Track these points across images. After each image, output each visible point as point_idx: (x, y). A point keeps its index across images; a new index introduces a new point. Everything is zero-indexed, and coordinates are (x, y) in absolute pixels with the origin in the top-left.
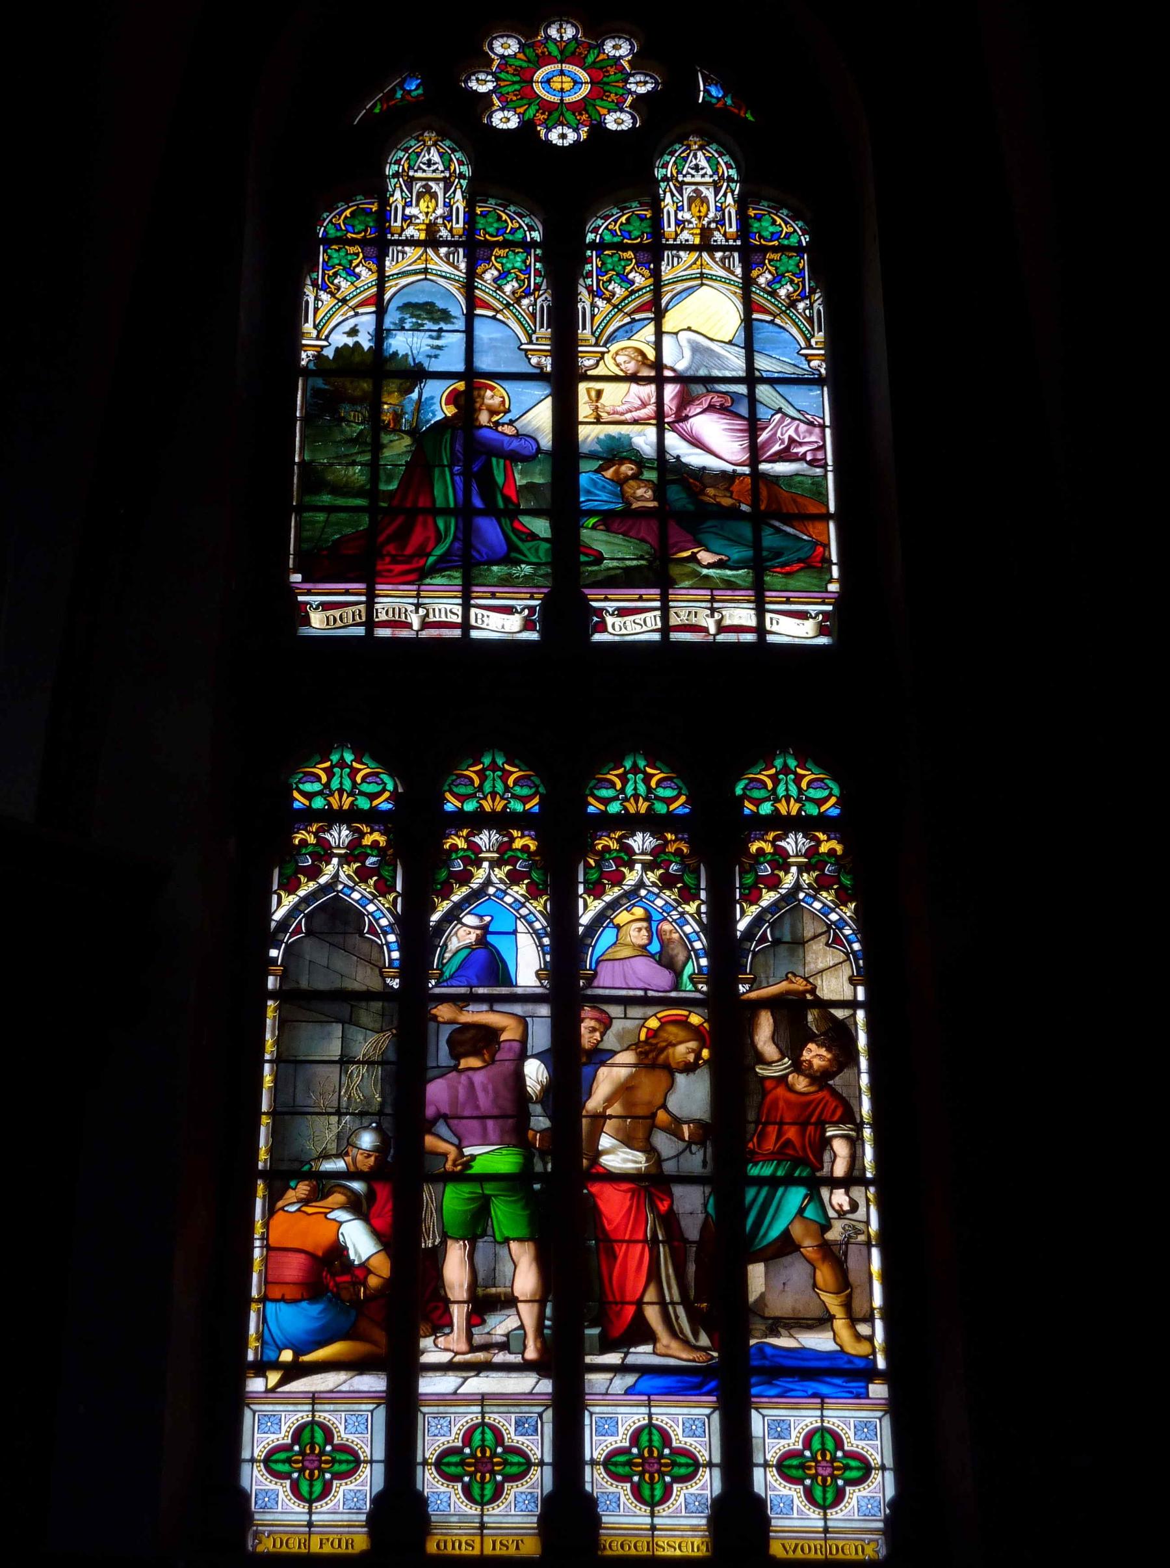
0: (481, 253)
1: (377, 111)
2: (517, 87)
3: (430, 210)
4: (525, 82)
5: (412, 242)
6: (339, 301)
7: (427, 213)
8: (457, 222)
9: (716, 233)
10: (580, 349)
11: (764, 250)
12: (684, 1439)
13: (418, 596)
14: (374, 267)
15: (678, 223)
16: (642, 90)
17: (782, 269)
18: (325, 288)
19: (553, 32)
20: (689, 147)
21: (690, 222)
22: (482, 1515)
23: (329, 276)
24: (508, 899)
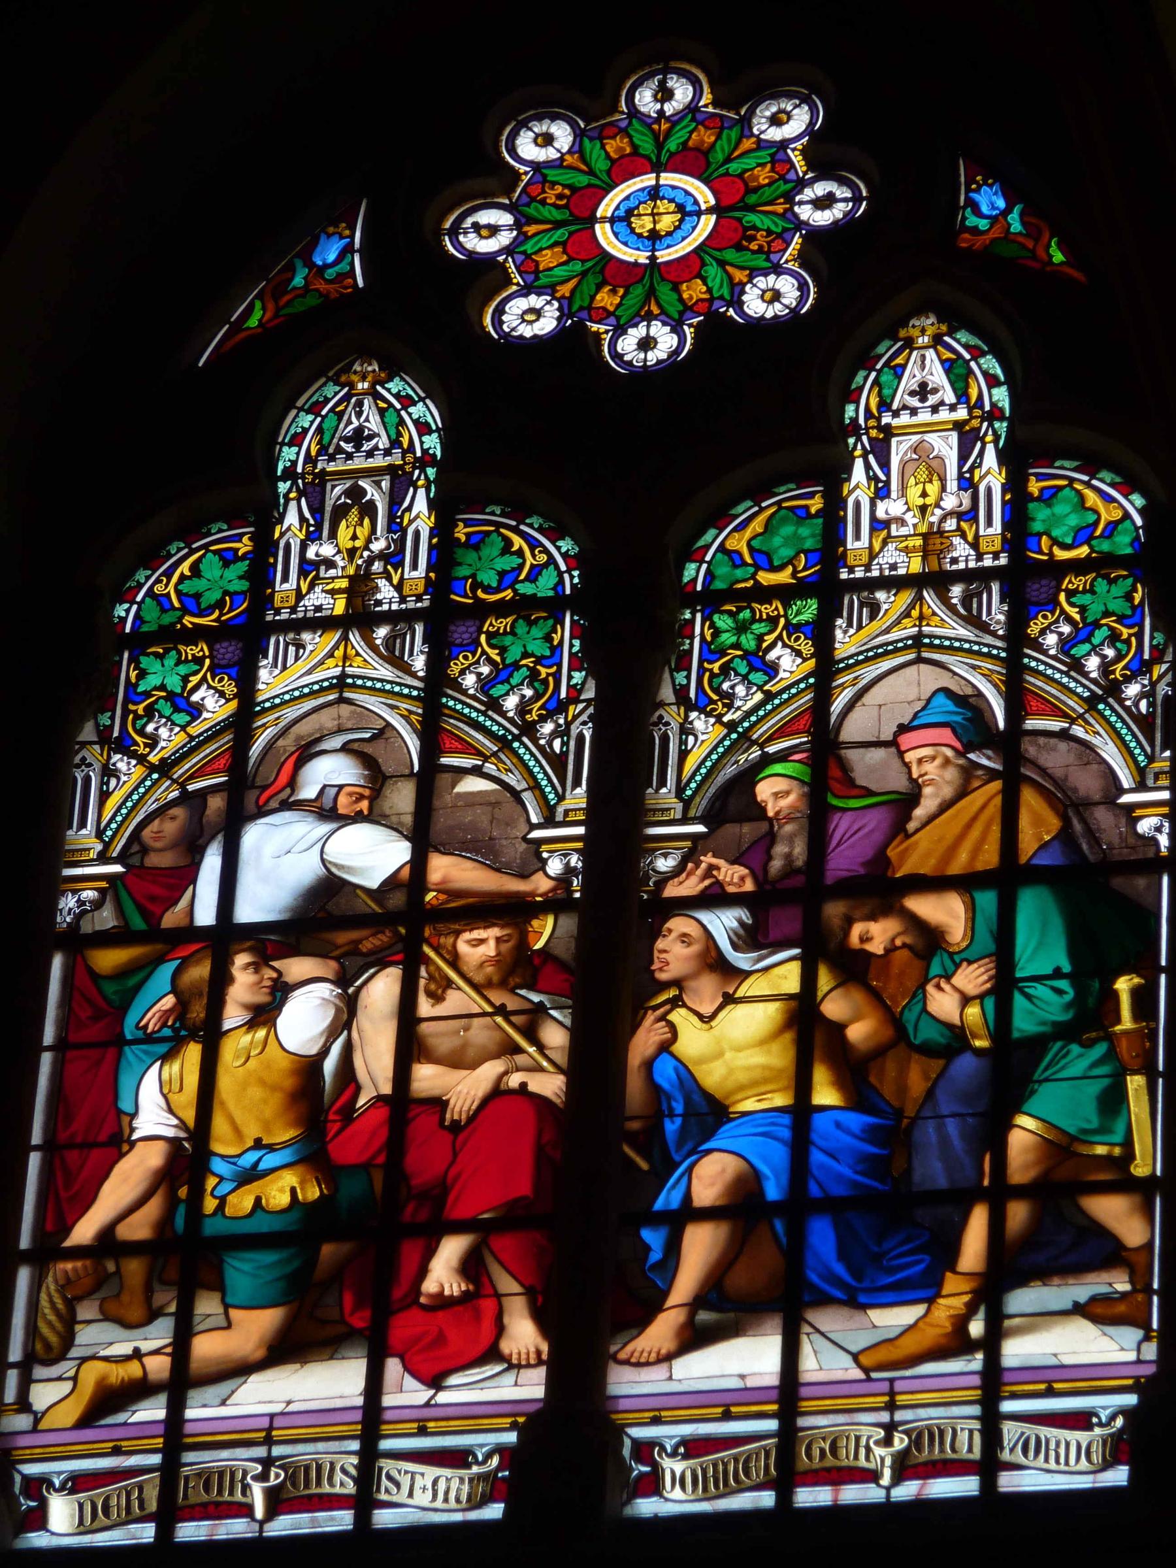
1: (253, 322)
4: (576, 220)
5: (322, 623)
6: (152, 768)
7: (923, 509)
8: (989, 523)
9: (382, 583)
10: (580, 830)
11: (482, 611)
14: (230, 688)
15: (878, 525)
16: (822, 218)
17: (1095, 611)
18: (124, 746)
20: (909, 344)
23: (713, 676)
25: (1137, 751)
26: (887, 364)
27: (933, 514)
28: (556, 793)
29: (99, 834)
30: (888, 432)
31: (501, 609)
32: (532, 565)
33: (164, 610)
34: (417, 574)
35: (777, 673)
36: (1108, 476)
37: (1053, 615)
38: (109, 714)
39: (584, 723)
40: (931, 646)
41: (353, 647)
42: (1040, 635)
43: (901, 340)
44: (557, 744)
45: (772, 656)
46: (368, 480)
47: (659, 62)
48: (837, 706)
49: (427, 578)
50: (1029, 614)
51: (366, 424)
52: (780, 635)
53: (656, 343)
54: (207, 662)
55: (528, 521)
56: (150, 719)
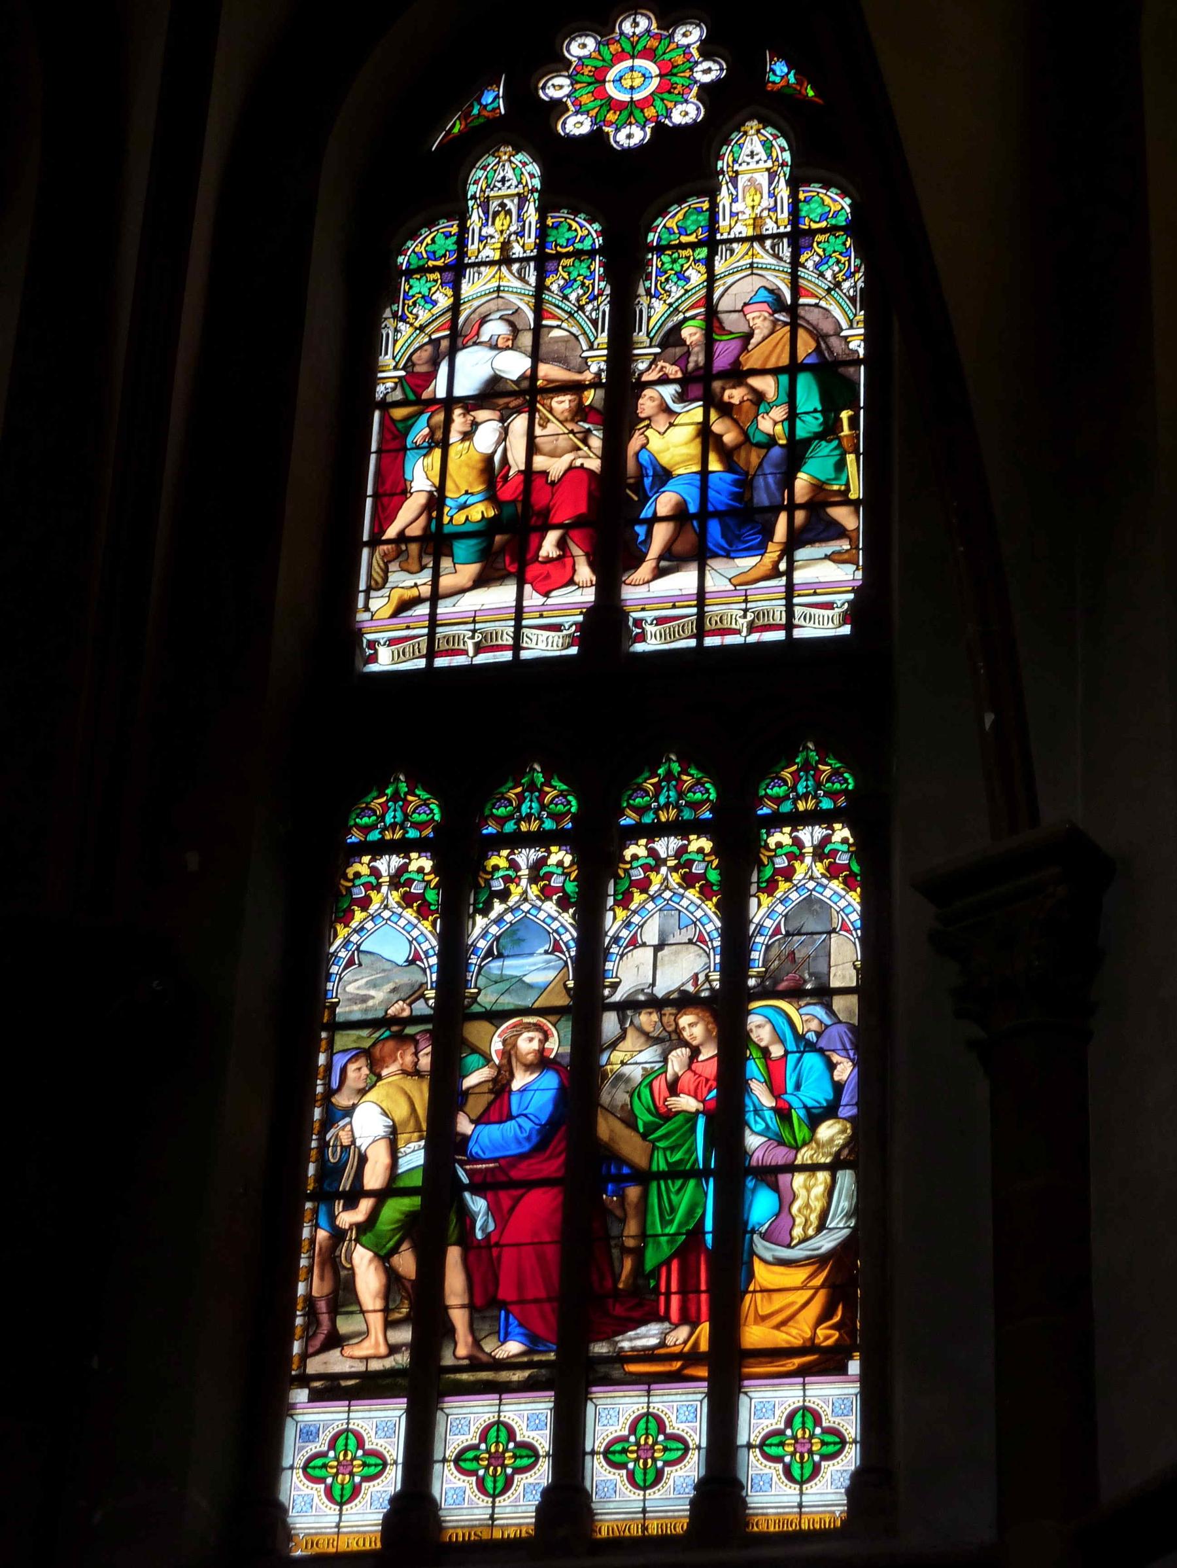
0: (803, 241)
2: (591, 88)
3: (505, 227)
4: (597, 81)
6: (416, 329)
7: (753, 207)
12: (527, 1434)
13: (746, 601)
14: (450, 293)
16: (706, 79)
17: (830, 250)
18: (403, 319)
19: (627, 27)
20: (745, 133)
21: (492, 237)
22: (644, 1500)
24: (402, 922)
31: (568, 255)
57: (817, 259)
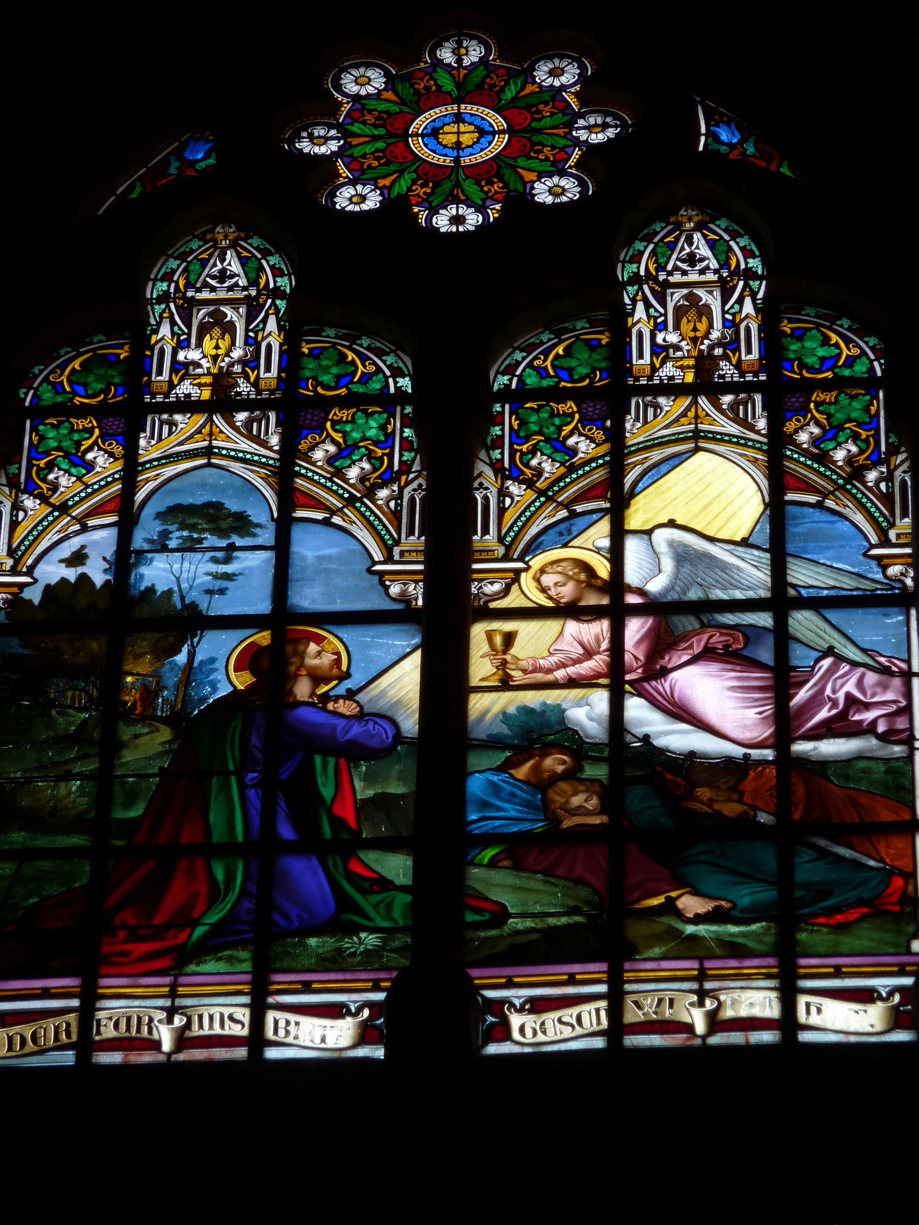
2: (380, 145)
3: (221, 352)
4: (390, 135)
6: (55, 508)
7: (215, 358)
14: (118, 450)
15: (656, 349)
16: (597, 138)
17: (840, 416)
18: (31, 489)
20: (678, 226)
23: (39, 469)
25: (387, 537)
26: (661, 240)
27: (223, 361)
28: (888, 522)
29: (501, 540)
30: (666, 285)
31: (825, 385)
32: (848, 356)
33: (57, 393)
34: (270, 375)
35: (94, 468)
36: (846, 323)
37: (320, 437)
38: (17, 466)
39: (904, 472)
40: (706, 438)
41: (217, 427)
42: (309, 451)
43: (671, 224)
44: (883, 486)
45: (90, 456)
46: (228, 307)
47: (459, 32)
48: (140, 496)
49: (279, 378)
50: (301, 434)
51: (228, 267)
52: (96, 441)
53: (465, 219)
54: (577, 416)
55: (838, 323)
56: (51, 471)
57: (332, 449)
